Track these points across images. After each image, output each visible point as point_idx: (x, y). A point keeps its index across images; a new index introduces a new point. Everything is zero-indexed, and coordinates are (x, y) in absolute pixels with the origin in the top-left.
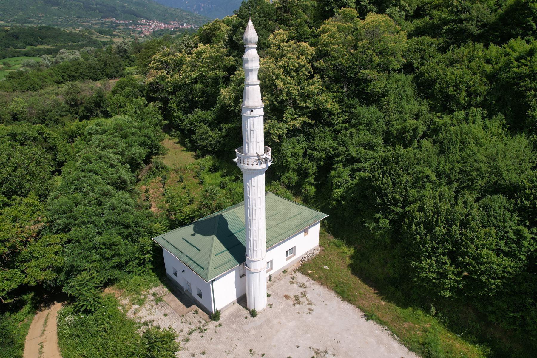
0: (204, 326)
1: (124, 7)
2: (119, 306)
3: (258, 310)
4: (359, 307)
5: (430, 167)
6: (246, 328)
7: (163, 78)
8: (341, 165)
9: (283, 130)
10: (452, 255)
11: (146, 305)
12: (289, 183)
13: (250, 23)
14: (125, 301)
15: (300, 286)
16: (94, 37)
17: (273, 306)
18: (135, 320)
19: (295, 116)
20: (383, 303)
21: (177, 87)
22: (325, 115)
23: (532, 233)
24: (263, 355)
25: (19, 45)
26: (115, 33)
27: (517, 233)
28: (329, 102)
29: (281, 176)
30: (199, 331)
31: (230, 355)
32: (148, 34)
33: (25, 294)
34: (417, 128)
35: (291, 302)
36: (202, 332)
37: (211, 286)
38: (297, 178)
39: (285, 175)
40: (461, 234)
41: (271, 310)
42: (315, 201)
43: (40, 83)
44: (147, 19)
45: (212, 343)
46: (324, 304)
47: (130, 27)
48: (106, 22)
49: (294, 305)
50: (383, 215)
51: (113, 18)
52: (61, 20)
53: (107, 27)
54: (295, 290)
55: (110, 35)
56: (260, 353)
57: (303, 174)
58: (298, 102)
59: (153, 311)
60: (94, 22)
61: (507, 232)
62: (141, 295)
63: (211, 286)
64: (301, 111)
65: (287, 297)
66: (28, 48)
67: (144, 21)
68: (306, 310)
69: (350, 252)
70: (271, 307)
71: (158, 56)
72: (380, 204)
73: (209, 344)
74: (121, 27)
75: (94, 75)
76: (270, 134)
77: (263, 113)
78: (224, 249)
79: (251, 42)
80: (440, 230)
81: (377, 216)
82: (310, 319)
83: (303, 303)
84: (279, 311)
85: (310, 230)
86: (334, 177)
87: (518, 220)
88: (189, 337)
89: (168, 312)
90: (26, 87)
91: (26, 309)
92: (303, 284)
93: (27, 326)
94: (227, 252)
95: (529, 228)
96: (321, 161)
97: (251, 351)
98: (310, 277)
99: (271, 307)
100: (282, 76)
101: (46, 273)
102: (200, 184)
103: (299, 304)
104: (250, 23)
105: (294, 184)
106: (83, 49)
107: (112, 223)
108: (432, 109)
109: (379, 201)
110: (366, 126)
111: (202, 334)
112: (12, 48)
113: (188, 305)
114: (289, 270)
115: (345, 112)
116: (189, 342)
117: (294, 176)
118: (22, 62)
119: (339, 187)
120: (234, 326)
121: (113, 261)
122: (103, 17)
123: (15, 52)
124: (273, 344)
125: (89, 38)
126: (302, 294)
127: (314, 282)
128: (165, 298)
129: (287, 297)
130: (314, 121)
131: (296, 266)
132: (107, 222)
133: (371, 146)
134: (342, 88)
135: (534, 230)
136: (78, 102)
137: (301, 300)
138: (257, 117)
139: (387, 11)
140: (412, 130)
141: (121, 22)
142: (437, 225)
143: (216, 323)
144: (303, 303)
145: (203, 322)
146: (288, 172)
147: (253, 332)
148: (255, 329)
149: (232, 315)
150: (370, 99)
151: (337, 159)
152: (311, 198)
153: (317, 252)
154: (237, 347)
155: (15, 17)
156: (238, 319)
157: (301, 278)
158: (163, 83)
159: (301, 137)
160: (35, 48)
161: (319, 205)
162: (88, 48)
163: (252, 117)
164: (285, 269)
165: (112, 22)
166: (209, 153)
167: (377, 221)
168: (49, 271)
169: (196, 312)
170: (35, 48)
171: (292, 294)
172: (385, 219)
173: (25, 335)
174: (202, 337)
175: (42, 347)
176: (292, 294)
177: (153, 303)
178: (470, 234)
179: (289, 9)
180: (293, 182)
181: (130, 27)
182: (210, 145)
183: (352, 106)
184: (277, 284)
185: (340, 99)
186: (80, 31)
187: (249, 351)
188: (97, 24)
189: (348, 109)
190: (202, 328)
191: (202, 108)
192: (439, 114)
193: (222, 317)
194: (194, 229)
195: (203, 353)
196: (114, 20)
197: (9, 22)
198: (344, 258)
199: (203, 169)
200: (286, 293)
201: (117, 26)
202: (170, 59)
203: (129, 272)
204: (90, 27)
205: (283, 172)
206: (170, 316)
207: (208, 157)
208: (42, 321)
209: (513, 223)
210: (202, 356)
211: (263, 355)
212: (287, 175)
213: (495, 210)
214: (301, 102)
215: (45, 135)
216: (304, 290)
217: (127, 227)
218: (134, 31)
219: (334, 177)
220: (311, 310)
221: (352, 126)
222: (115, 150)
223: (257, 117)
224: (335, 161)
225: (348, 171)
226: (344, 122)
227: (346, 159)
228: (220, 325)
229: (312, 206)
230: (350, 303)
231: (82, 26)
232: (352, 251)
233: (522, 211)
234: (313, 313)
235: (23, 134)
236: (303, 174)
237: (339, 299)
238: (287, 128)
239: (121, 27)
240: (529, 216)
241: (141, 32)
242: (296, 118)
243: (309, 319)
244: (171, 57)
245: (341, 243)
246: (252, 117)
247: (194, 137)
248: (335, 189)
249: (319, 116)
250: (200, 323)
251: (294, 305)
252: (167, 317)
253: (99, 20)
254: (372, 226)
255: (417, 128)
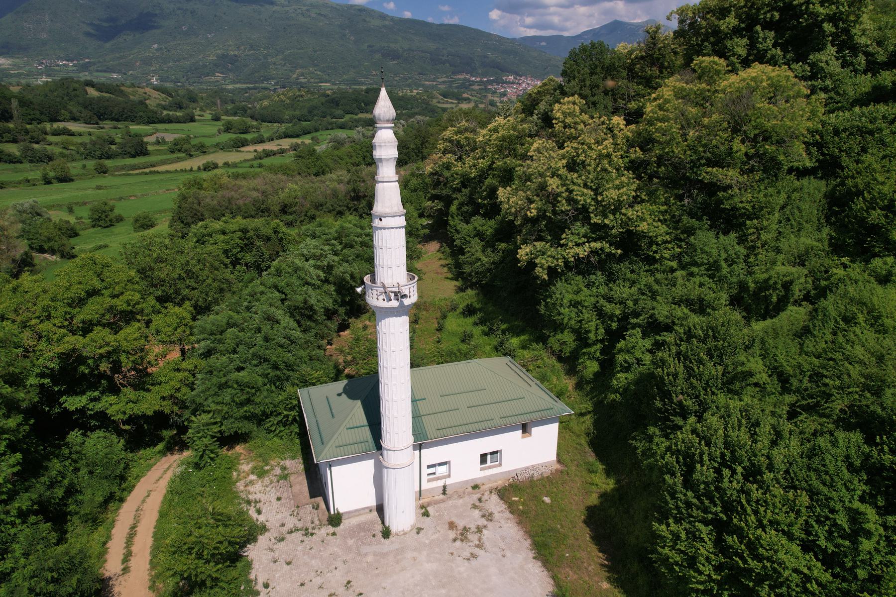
0: (313, 528)
1: (486, 57)
2: (236, 470)
3: (394, 529)
4: (554, 578)
5: (765, 357)
6: (364, 549)
7: (448, 167)
8: (638, 332)
9: (557, 260)
10: (721, 527)
11: (267, 479)
12: (561, 351)
13: (383, 92)
14: (245, 467)
15: (483, 516)
16: (435, 101)
17: (422, 533)
18: (241, 494)
19: (584, 240)
20: (605, 585)
21: (466, 181)
22: (643, 244)
23: (885, 527)
24: (361, 594)
25: (339, 112)
26: (465, 95)
27: (855, 516)
28: (647, 220)
29: (549, 336)
30: (304, 533)
31: (319, 578)
32: (514, 98)
33: (165, 429)
34: (791, 282)
35: (452, 534)
36: (306, 535)
37: (328, 472)
38: (573, 345)
39: (557, 337)
40: (742, 491)
41: (416, 536)
42: (592, 388)
43: (332, 165)
44: (517, 74)
45: (308, 554)
46: (500, 555)
47: (490, 87)
48: (456, 80)
49: (455, 540)
50: (661, 430)
51: (467, 74)
52: (397, 78)
53: (457, 87)
54: (475, 518)
55: (458, 99)
56: (357, 591)
57: (582, 339)
58: (592, 215)
59: (268, 489)
60: (440, 80)
61: (833, 511)
62: (267, 464)
63: (328, 472)
64: (599, 232)
65: (452, 526)
66: (348, 117)
67: (511, 78)
68: (467, 554)
69: (604, 486)
70: (418, 533)
71: (448, 133)
72: (659, 410)
73: (304, 554)
74: (476, 87)
75: (405, 157)
76: (535, 265)
77: (405, 223)
78: (366, 423)
79: (380, 120)
80: (704, 472)
81: (652, 430)
82: (462, 569)
83: (470, 541)
84: (427, 542)
85: (534, 430)
86: (621, 351)
87: (864, 491)
88: (288, 536)
89: (285, 495)
90: (314, 170)
91: (160, 446)
92: (491, 514)
93: (150, 467)
94: (367, 429)
95: (883, 512)
96: (613, 321)
97: (349, 582)
98: (509, 507)
99: (418, 533)
100: (563, 172)
101: (165, 403)
102: (437, 330)
103: (462, 540)
104: (383, 92)
105: (568, 354)
106: (413, 119)
107: (261, 358)
108: (837, 248)
109: (658, 404)
110: (707, 270)
111: (305, 538)
112: (329, 118)
113: (313, 495)
114: (482, 488)
115: (681, 240)
116: (282, 543)
117: (568, 337)
118: (329, 137)
119: (627, 369)
120: (351, 542)
121: (245, 408)
122: (454, 73)
123: (332, 123)
124: (384, 585)
125: (428, 104)
126: (478, 527)
127: (510, 516)
128: (292, 478)
129: (452, 526)
130: (619, 251)
131: (499, 483)
132: (254, 355)
133: (701, 307)
134: (680, 198)
135: (891, 519)
136: (361, 194)
137: (470, 536)
138: (385, 229)
139: (811, 57)
140: (782, 286)
141: (478, 80)
142: (701, 462)
143: (331, 529)
144: (470, 541)
145: (317, 522)
146: (562, 333)
147: (370, 559)
148: (375, 554)
149: (359, 525)
150: (728, 221)
151: (632, 321)
152: (588, 383)
153: (547, 472)
154: (334, 571)
155: (345, 77)
156: (362, 534)
157: (495, 504)
158: (447, 174)
159: (598, 277)
160: (356, 117)
161: (596, 396)
162: (419, 117)
163: (381, 229)
164: (478, 482)
165: (465, 79)
166: (472, 286)
167: (650, 439)
168: (169, 402)
169: (316, 507)
170: (356, 117)
171: (461, 524)
172: (663, 439)
173: (142, 477)
174: (302, 541)
175: (148, 496)
176: (461, 524)
177: (275, 479)
178: (756, 494)
179: (658, 59)
180: (567, 351)
181: (490, 87)
182: (477, 273)
183: (690, 231)
184: (450, 503)
185: (674, 216)
186: (417, 93)
187: (345, 582)
188: (444, 82)
189: (682, 234)
190: (310, 531)
191: (484, 216)
192: (846, 260)
193: (345, 524)
194: (345, 388)
195: (288, 563)
196: (468, 77)
197: (336, 84)
198: (588, 493)
199: (454, 309)
200: (454, 519)
201: (471, 85)
202: (466, 138)
203: (269, 431)
204: (433, 87)
205: (555, 331)
206: (283, 501)
207: (470, 292)
208: (167, 465)
209: (850, 495)
210: (285, 566)
211: (361, 594)
212: (559, 336)
213: (823, 460)
214: (596, 216)
215: (281, 235)
216: (485, 523)
217: (275, 367)
218: (494, 92)
219: (621, 351)
220: (474, 556)
221: (683, 267)
222: (319, 263)
223: (385, 229)
224: (630, 323)
225: (648, 343)
226: (673, 257)
227: (648, 322)
228: (334, 534)
229: (587, 395)
230: (545, 566)
231: (423, 86)
232: (609, 485)
233: (873, 472)
234: (474, 562)
235: (256, 230)
236: (582, 339)
237: (531, 554)
238: (564, 258)
239: (476, 87)
240: (887, 487)
241: (504, 94)
242: (584, 243)
243: (462, 568)
244: (467, 134)
245: (600, 467)
246: (381, 229)
247: (462, 258)
248: (619, 372)
249: (631, 244)
250: (313, 523)
251: (455, 540)
252: (279, 502)
253: (447, 77)
254: (640, 446)
255: (791, 282)
